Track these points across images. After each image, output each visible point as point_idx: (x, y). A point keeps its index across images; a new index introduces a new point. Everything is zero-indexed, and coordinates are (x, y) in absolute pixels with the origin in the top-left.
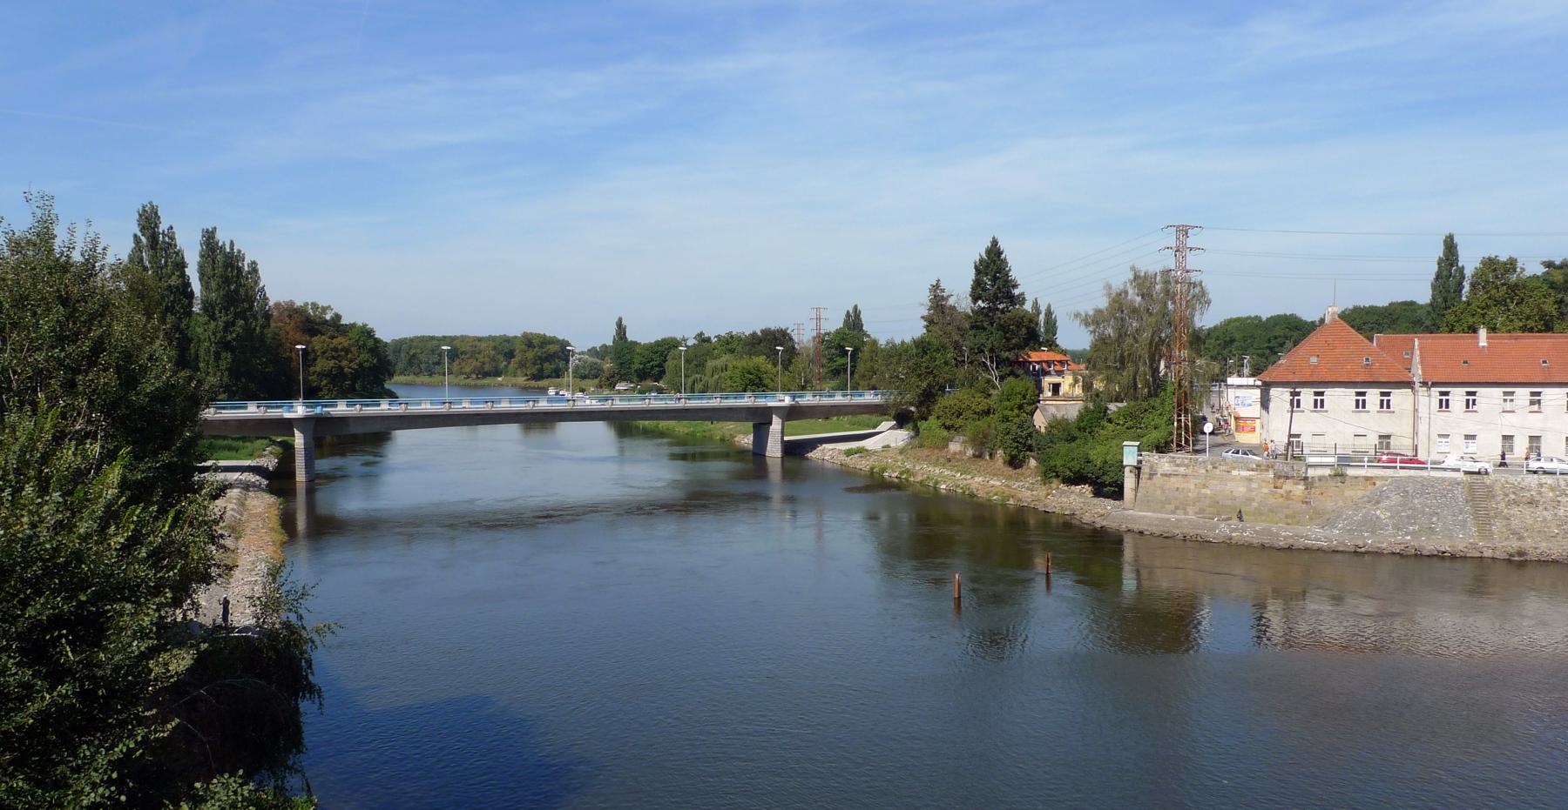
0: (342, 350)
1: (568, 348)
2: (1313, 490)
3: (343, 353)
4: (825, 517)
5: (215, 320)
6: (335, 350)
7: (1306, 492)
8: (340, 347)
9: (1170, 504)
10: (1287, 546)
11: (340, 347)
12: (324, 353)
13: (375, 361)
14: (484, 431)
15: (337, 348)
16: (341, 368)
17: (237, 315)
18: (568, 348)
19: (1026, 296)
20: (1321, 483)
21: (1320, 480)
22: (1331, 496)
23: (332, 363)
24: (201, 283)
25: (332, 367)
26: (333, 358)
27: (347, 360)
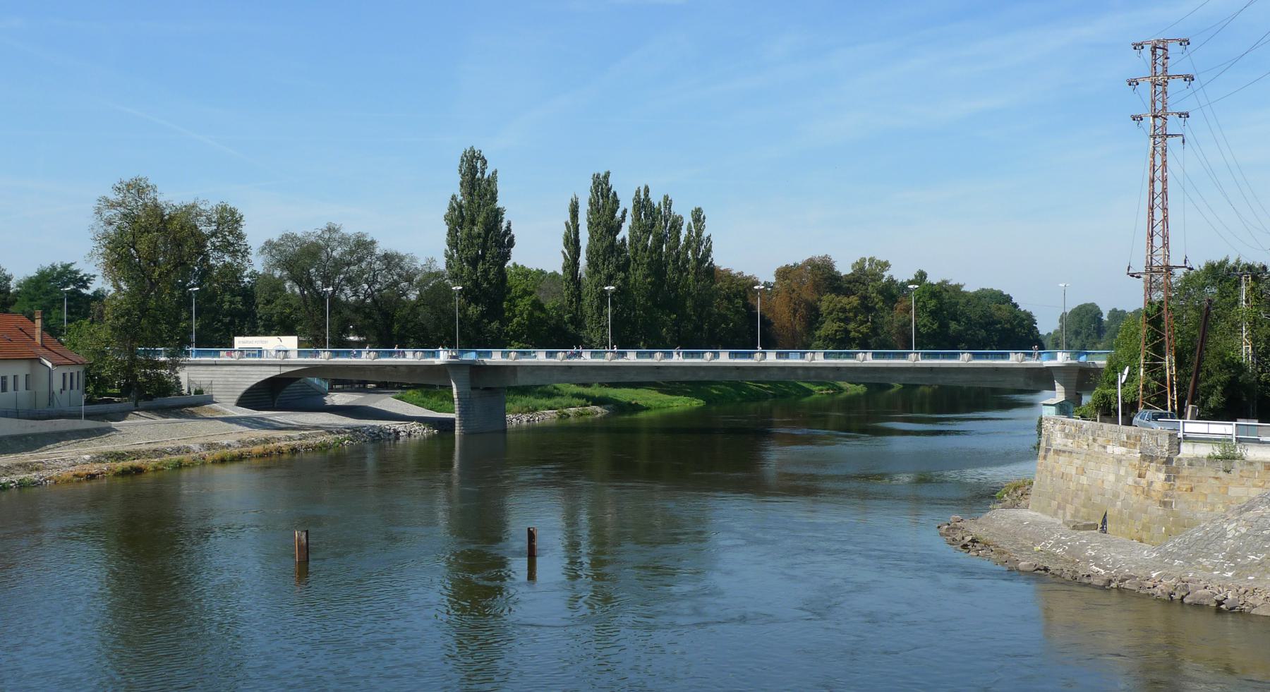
0: (850, 311)
1: (756, 287)
2: (1178, 483)
3: (851, 314)
4: (15, 408)
5: (599, 272)
6: (843, 310)
7: (1167, 485)
8: (848, 307)
9: (1055, 500)
10: (1032, 568)
11: (848, 307)
12: (830, 313)
13: (935, 326)
14: (989, 421)
15: (845, 308)
16: (847, 332)
17: (618, 268)
18: (756, 287)
19: (456, 194)
20: (1193, 470)
21: (1190, 464)
22: (1206, 495)
23: (835, 326)
24: (452, 234)
25: (836, 331)
26: (840, 320)
27: (856, 322)
